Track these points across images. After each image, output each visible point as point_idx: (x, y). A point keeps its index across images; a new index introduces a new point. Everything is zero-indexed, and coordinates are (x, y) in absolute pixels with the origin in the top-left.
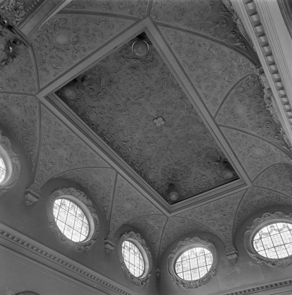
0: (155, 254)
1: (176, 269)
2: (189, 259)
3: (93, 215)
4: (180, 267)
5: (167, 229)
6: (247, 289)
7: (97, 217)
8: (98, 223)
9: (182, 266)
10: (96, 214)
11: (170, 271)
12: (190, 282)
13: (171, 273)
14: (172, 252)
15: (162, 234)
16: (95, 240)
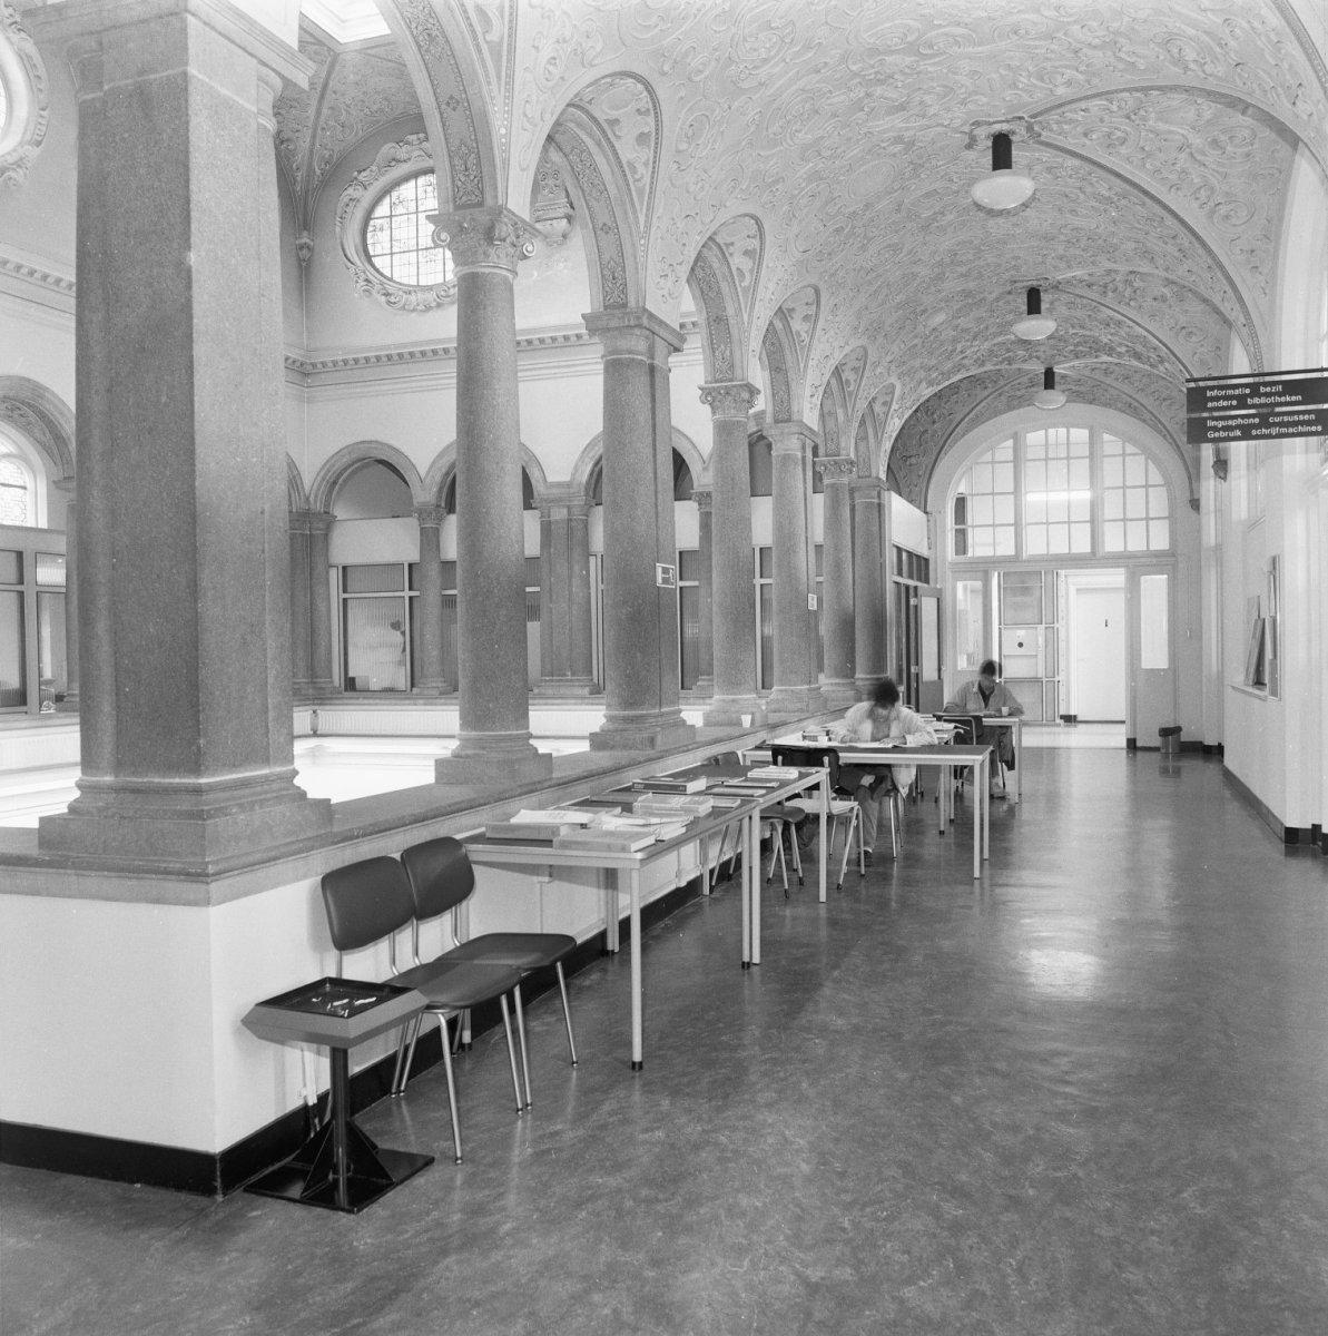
0: (295, 181)
1: (369, 241)
2: (417, 212)
3: (15, 37)
4: (384, 236)
5: (334, 92)
6: (374, 354)
7: (30, 47)
8: (42, 71)
9: (389, 232)
10: (23, 35)
11: (346, 247)
12: (410, 290)
13: (349, 255)
14: (356, 178)
15: (319, 112)
16: (39, 144)
